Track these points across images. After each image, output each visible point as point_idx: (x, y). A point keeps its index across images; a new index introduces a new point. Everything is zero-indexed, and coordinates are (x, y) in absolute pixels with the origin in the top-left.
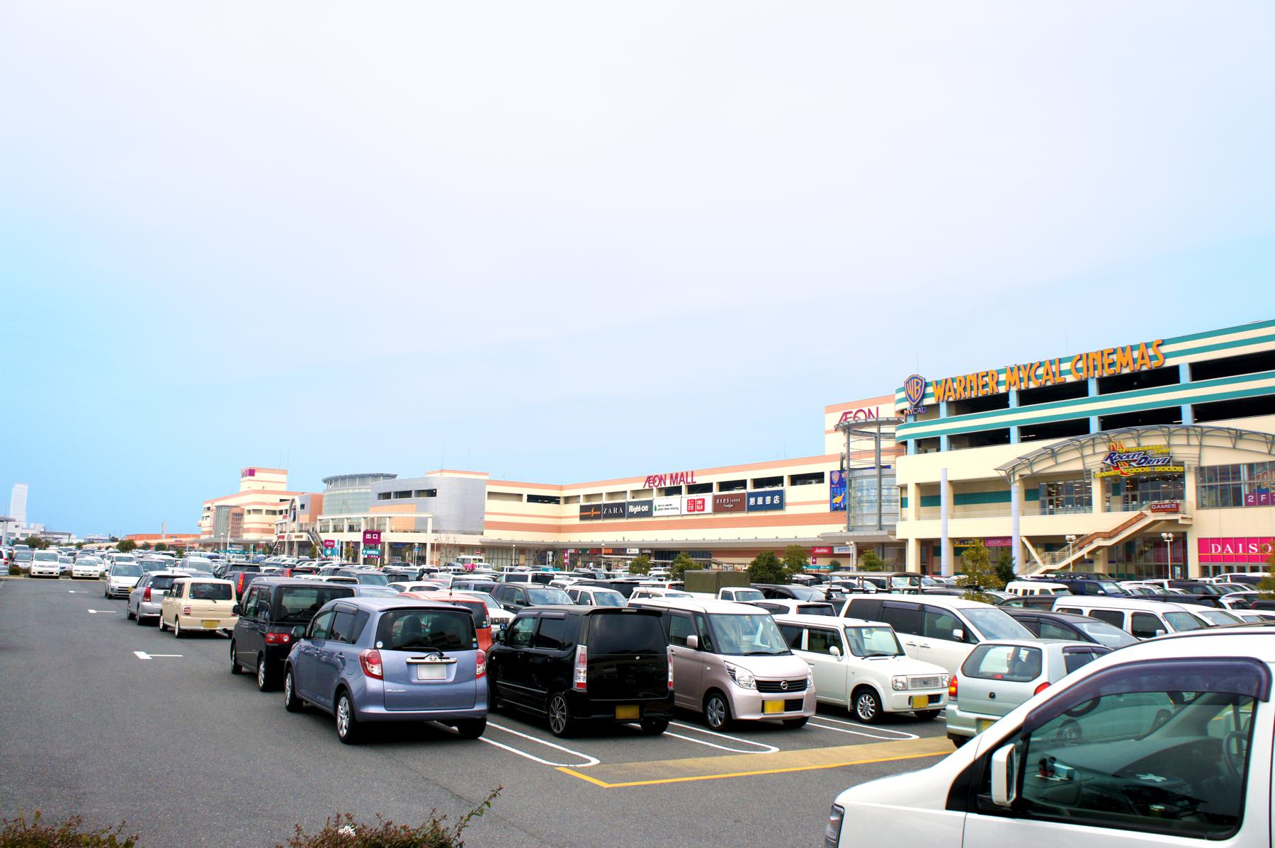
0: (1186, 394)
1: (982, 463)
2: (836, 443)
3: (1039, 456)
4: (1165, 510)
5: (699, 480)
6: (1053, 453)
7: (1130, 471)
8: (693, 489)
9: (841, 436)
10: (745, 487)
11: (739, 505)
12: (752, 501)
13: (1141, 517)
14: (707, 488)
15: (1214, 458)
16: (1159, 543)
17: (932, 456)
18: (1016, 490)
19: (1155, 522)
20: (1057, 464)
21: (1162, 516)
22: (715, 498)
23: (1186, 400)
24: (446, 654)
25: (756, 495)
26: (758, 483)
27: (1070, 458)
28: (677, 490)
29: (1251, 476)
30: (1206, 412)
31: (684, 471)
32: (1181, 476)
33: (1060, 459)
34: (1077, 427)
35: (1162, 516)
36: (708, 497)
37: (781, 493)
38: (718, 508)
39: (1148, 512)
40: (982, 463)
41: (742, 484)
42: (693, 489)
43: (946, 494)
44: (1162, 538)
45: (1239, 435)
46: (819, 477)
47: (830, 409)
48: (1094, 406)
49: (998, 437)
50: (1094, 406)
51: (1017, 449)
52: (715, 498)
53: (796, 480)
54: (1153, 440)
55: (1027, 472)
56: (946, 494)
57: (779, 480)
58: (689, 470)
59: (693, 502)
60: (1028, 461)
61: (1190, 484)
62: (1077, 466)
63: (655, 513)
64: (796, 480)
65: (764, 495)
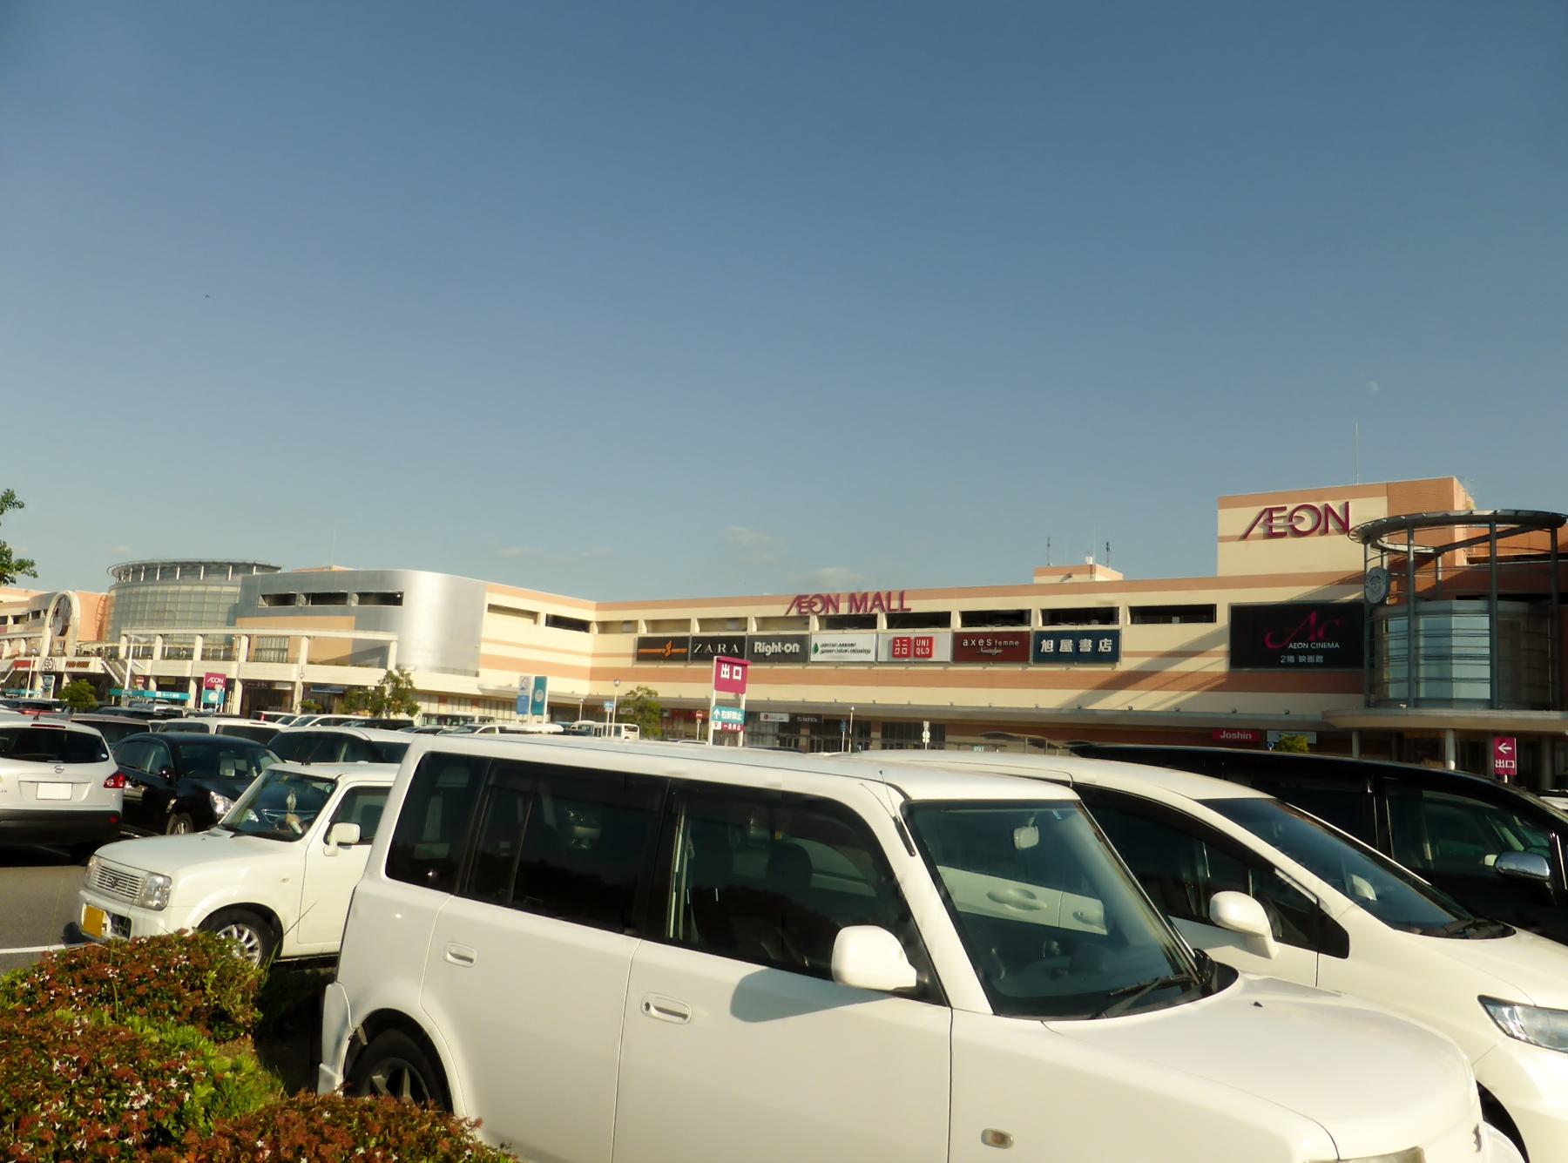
5: (917, 606)
8: (897, 620)
10: (1028, 623)
14: (941, 619)
22: (958, 638)
26: (1052, 616)
28: (869, 622)
31: (884, 590)
38: (964, 651)
41: (1021, 617)
42: (897, 620)
46: (1205, 613)
52: (958, 638)
53: (1144, 615)
57: (1109, 615)
58: (896, 588)
63: (814, 657)
64: (1144, 615)
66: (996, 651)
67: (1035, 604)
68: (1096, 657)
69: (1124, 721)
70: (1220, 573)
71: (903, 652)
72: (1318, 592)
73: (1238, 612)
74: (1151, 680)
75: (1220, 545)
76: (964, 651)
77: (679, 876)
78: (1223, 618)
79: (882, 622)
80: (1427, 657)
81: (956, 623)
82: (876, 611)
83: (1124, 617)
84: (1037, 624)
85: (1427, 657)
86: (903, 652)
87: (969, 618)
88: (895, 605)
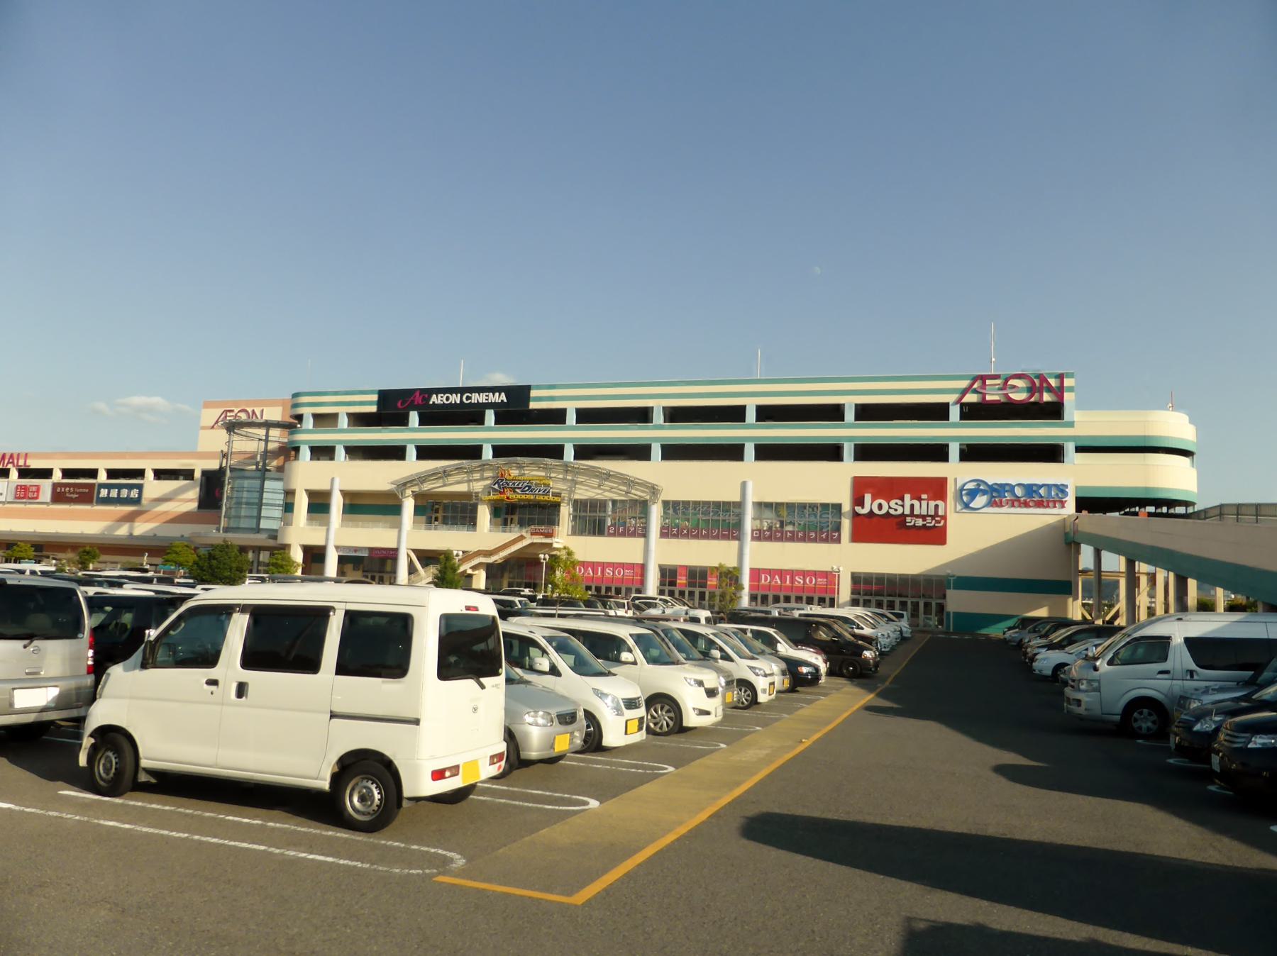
0: (750, 433)
1: (377, 477)
2: (217, 440)
3: (433, 475)
4: (542, 534)
5: (34, 464)
6: (446, 473)
7: (515, 497)
8: (25, 473)
9: (223, 433)
11: (87, 496)
12: (104, 493)
13: (522, 538)
14: (46, 474)
15: (583, 493)
16: (537, 563)
17: (323, 464)
18: (409, 505)
19: (532, 544)
20: (445, 485)
21: (538, 539)
22: (55, 486)
23: (955, 425)
24: (1003, 400)
25: (109, 487)
26: (112, 473)
27: (458, 481)
29: (614, 510)
30: (584, 452)
31: (15, 451)
32: (556, 506)
33: (451, 480)
34: (473, 452)
35: (538, 539)
36: (46, 486)
37: (140, 487)
39: (527, 535)
40: (377, 477)
41: (93, 473)
42: (25, 473)
43: (337, 503)
44: (539, 559)
45: (608, 476)
46: (188, 474)
47: (208, 405)
48: (849, 432)
49: (396, 453)
50: (849, 432)
51: (412, 466)
52: (55, 486)
53: (160, 474)
54: (531, 471)
55: (416, 489)
56: (337, 503)
57: (140, 473)
58: (23, 450)
59: (24, 488)
60: (423, 478)
61: (566, 511)
62: (463, 488)
64: (160, 474)
65: (120, 487)
66: (75, 496)
67: (102, 466)
68: (128, 501)
69: (126, 542)
70: (199, 449)
71: (24, 494)
72: (1213, 631)
73: (204, 473)
74: (169, 517)
75: (202, 432)
76: (59, 496)
77: (157, 592)
78: (198, 475)
79: (14, 474)
80: (247, 504)
81: (57, 476)
82: (10, 466)
83: (150, 475)
84: (102, 477)
85: (247, 504)
86: (24, 494)
87: (67, 473)
88: (21, 463)
